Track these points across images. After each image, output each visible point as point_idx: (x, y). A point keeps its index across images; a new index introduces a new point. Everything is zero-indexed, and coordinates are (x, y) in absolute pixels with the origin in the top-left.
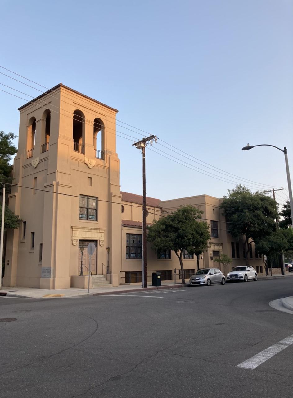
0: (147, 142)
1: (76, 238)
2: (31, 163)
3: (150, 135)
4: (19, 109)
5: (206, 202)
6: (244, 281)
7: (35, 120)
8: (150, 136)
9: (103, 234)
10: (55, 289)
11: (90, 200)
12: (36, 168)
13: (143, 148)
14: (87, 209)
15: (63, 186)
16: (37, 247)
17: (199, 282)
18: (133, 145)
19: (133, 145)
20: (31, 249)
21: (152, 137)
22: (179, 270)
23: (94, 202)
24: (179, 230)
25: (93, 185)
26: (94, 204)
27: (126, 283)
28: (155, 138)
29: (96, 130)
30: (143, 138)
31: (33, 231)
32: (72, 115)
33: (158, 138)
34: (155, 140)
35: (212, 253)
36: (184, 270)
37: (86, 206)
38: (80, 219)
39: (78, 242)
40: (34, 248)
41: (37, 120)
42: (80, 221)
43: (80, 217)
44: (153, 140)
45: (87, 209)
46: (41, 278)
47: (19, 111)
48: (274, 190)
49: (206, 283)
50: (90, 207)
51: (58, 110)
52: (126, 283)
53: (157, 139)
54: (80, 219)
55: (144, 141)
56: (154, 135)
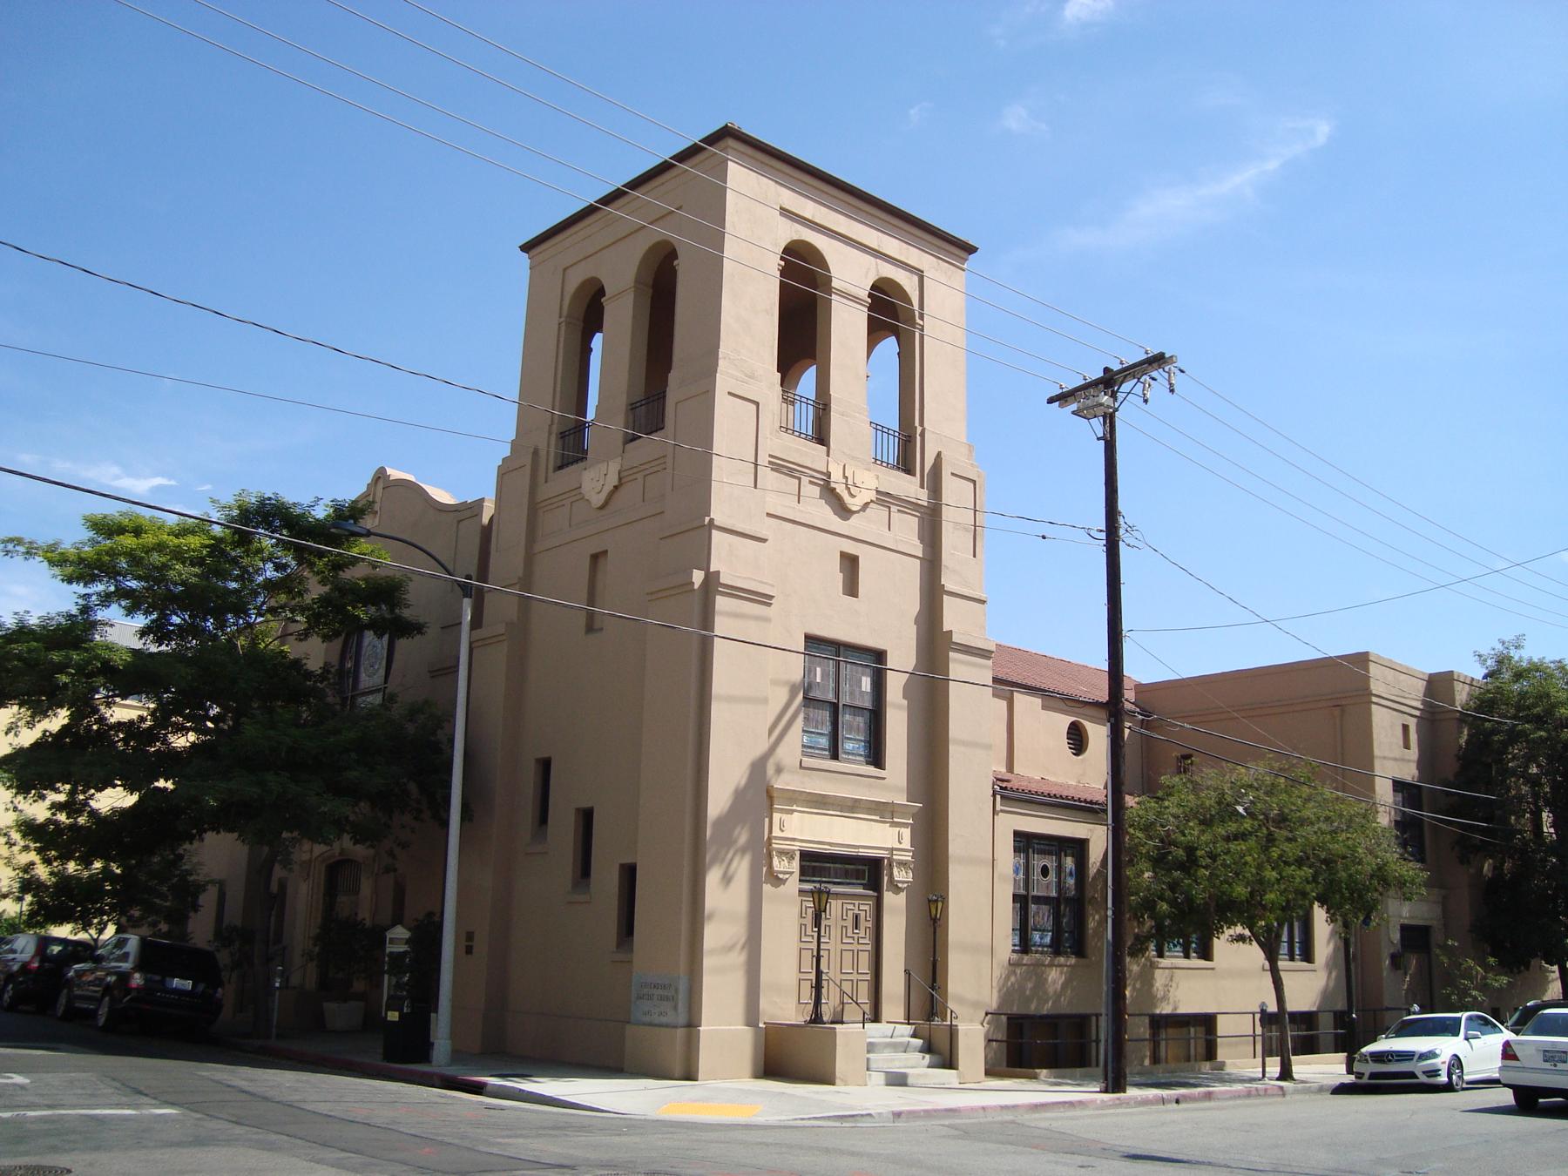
0: (1126, 387)
1: (785, 846)
2: (580, 487)
3: (1147, 353)
4: (526, 248)
5: (1376, 687)
6: (1448, 1088)
7: (601, 292)
8: (1145, 357)
9: (907, 833)
10: (700, 1078)
11: (846, 670)
12: (602, 508)
13: (1109, 419)
14: (834, 708)
15: (736, 592)
16: (606, 878)
17: (1412, 1075)
18: (1051, 401)
19: (1051, 401)
20: (576, 885)
21: (1158, 360)
22: (1254, 1014)
23: (867, 676)
24: (187, 842)
25: (983, 596)
26: (866, 684)
27: (1008, 1066)
28: (1167, 369)
29: (876, 331)
30: (1106, 370)
31: (586, 805)
32: (774, 264)
33: (1182, 371)
34: (1166, 375)
35: (1396, 936)
36: (1293, 1015)
37: (831, 697)
38: (804, 754)
39: (795, 866)
40: (588, 885)
41: (607, 296)
42: (807, 761)
43: (803, 746)
44: (1154, 379)
45: (834, 708)
46: (628, 1022)
47: (526, 255)
48: (403, 644)
49: (1443, 1079)
50: (845, 699)
51: (718, 240)
52: (1008, 1066)
53: (1178, 372)
54: (804, 754)
55: (1109, 381)
56: (1167, 356)
